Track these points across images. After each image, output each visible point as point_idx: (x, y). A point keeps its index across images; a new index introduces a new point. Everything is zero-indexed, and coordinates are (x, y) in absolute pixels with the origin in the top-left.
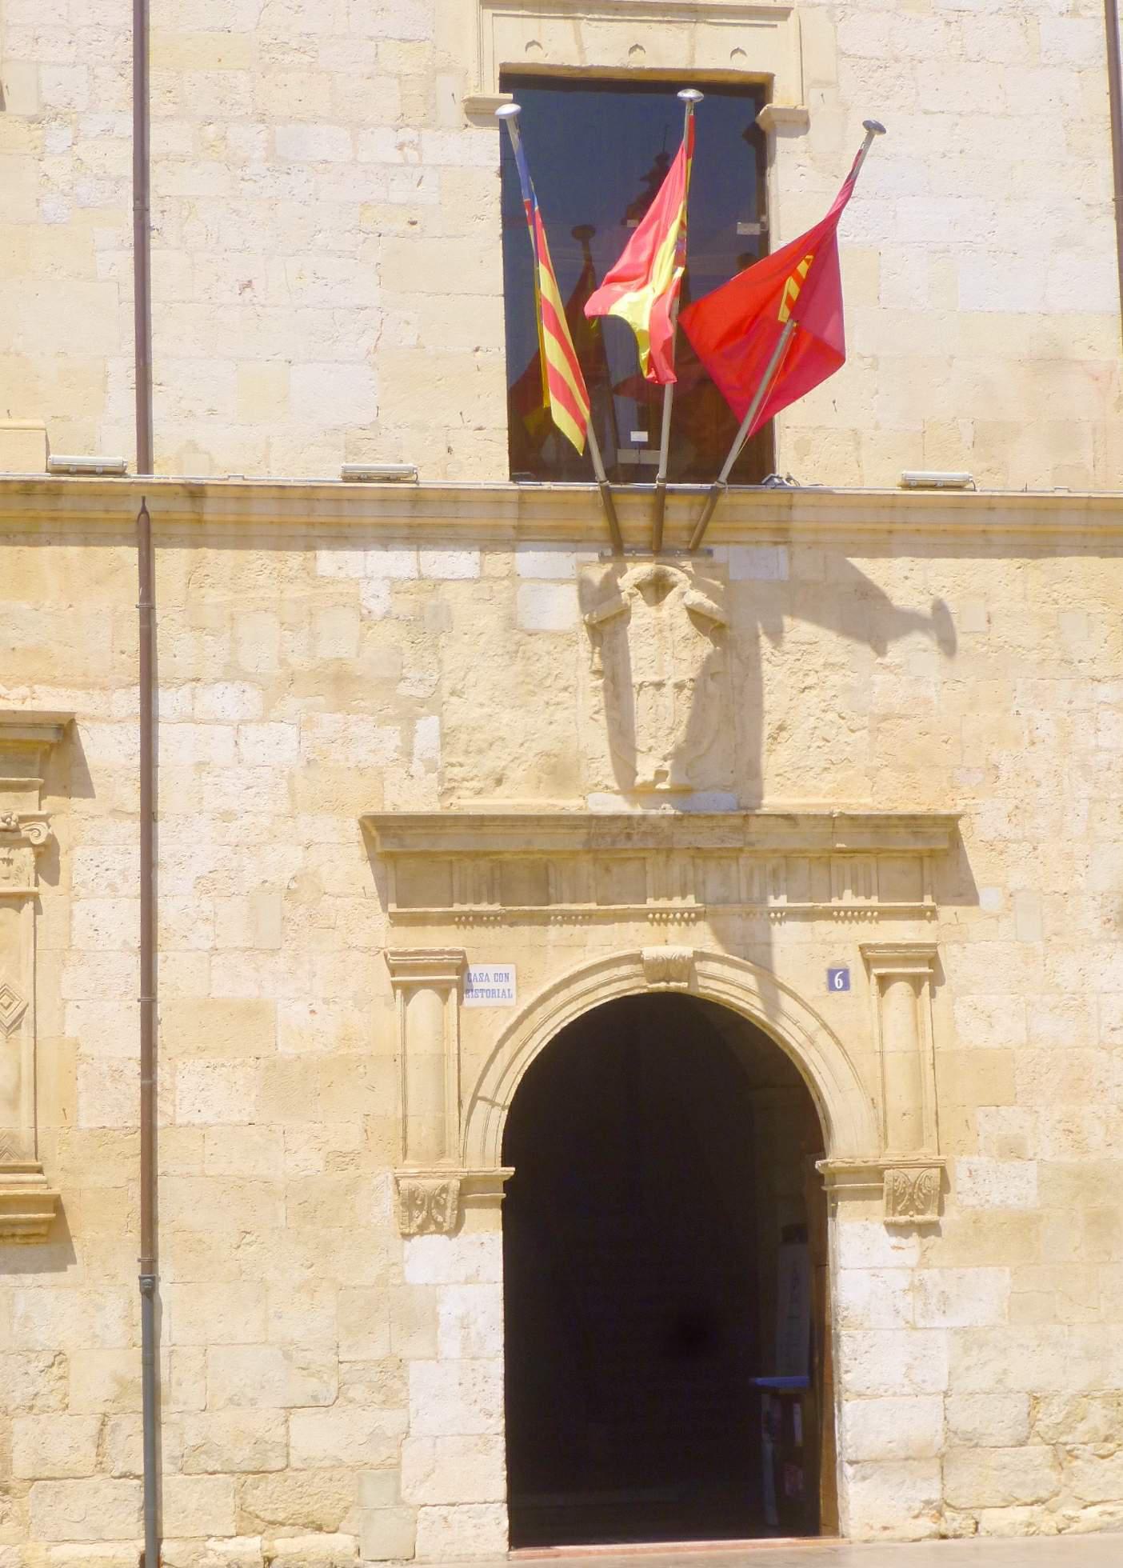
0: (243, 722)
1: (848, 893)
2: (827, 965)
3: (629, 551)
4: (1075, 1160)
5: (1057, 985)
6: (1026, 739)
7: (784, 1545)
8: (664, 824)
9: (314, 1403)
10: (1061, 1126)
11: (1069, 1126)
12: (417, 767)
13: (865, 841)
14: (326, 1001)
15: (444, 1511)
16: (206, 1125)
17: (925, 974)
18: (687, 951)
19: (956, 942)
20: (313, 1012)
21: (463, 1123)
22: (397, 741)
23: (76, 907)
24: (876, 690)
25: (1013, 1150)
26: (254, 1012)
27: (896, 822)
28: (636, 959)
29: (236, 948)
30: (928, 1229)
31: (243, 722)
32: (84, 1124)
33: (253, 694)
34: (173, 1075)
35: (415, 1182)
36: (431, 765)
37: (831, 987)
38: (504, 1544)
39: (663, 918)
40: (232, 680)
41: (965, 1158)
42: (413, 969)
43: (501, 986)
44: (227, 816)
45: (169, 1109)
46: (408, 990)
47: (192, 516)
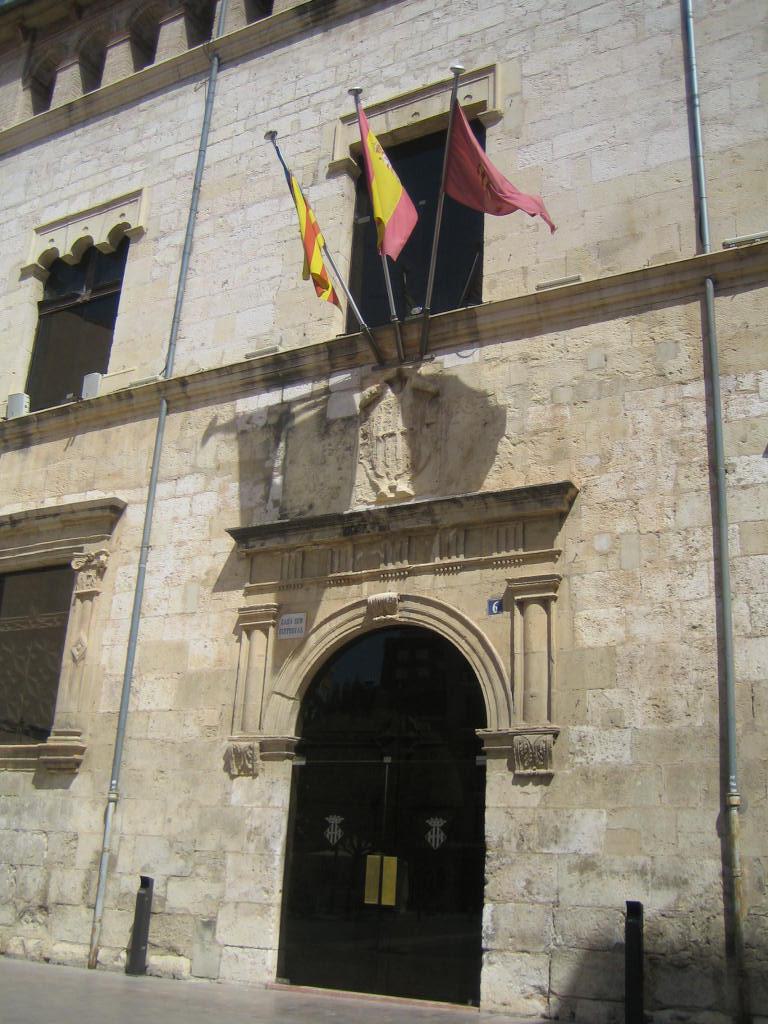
0: (195, 494)
1: (406, 562)
2: (488, 597)
3: (437, 342)
4: (660, 728)
5: (650, 598)
6: (631, 431)
7: (433, 1006)
8: (382, 516)
9: (181, 877)
10: (651, 702)
11: (655, 702)
12: (270, 504)
13: (508, 511)
14: (212, 640)
15: (238, 951)
16: (151, 711)
17: (269, 624)
18: (394, 595)
19: (578, 574)
20: (206, 646)
21: (510, 693)
22: (262, 492)
23: (114, 597)
24: (530, 416)
25: (614, 722)
26: (180, 648)
27: (525, 494)
28: (364, 602)
29: (176, 614)
30: (546, 779)
31: (195, 494)
32: (102, 711)
33: (201, 479)
34: (140, 684)
35: (235, 743)
36: (276, 503)
37: (491, 612)
38: (272, 977)
39: (383, 577)
40: (193, 474)
41: (576, 728)
42: (250, 618)
43: (298, 626)
44: (181, 544)
45: (136, 702)
46: (249, 631)
47: (183, 395)
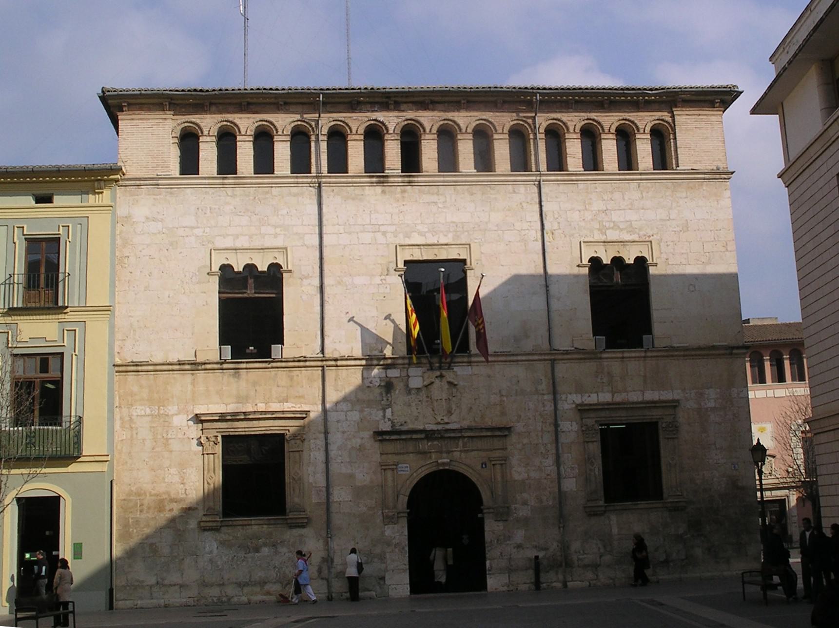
12: (386, 420)
25: (525, 503)
44: (344, 432)
